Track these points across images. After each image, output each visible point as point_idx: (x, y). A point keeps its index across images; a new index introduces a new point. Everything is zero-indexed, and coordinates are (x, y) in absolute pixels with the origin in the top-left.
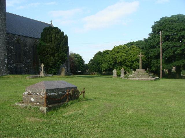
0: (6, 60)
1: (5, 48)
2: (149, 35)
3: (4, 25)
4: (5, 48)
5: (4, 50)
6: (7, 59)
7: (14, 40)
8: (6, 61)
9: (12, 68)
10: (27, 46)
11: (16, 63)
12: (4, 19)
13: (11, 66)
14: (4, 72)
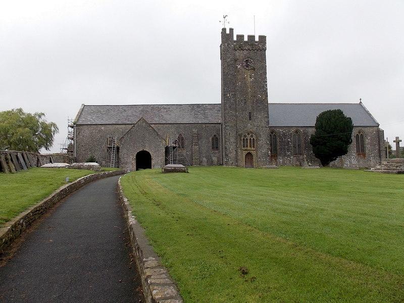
0: (270, 152)
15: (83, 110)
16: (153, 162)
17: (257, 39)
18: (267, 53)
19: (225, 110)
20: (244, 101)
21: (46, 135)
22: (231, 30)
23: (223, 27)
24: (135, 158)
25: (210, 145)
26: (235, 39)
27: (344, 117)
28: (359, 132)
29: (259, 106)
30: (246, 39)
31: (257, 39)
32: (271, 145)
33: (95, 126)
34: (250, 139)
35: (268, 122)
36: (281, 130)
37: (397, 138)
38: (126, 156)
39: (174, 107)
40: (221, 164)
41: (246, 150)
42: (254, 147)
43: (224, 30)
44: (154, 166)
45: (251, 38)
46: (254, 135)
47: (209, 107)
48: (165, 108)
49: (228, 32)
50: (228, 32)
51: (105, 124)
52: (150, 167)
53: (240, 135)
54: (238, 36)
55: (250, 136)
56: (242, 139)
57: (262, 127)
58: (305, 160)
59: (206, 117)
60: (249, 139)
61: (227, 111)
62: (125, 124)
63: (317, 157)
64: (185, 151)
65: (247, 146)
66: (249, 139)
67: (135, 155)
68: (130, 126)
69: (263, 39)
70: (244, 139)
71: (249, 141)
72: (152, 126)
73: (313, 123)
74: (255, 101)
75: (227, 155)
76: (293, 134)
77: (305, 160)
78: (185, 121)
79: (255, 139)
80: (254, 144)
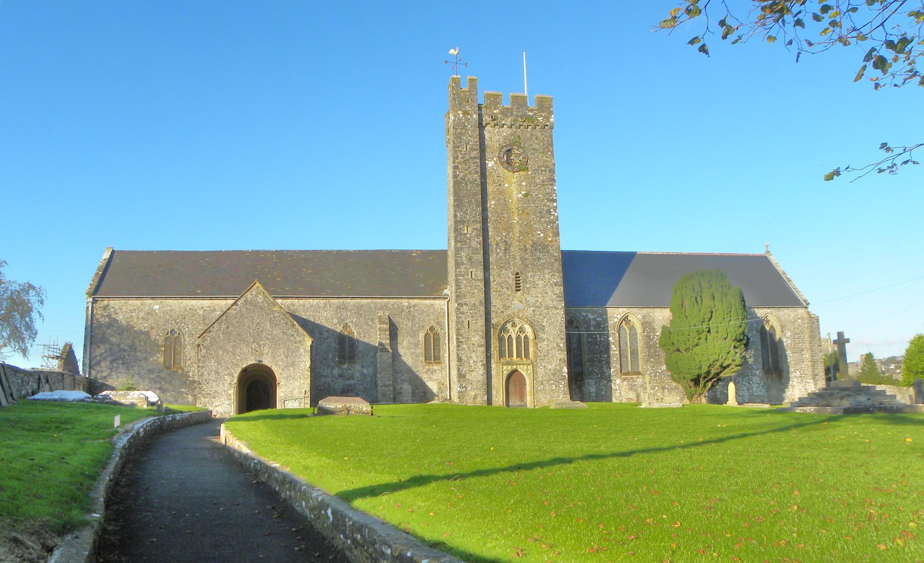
15: (109, 261)
24: (235, 381)
25: (421, 350)
29: (539, 259)
34: (518, 337)
37: (840, 335)
38: (213, 376)
40: (552, 171)
55: (517, 329)
57: (547, 308)
60: (514, 337)
61: (463, 268)
63: (674, 380)
64: (357, 367)
66: (514, 337)
74: (528, 246)
79: (531, 336)
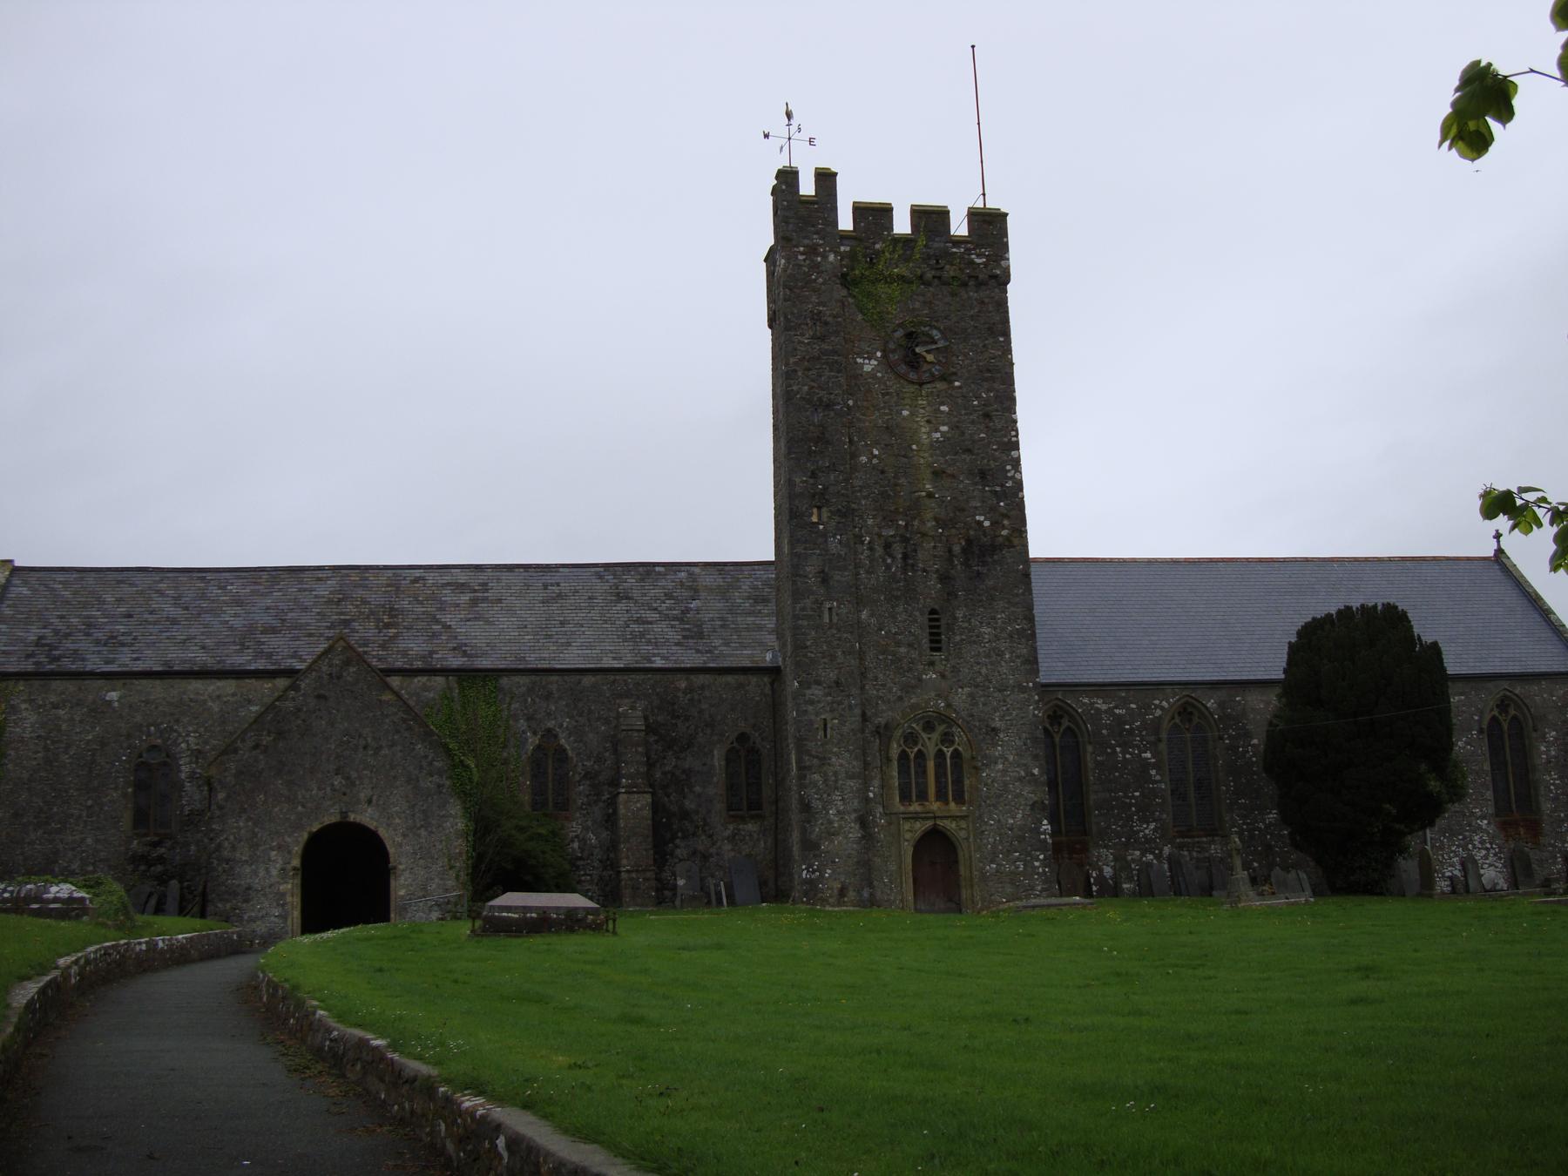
0: (1046, 826)
1: (1036, 771)
2: (1552, 526)
3: (1023, 663)
4: (1036, 771)
5: (1033, 780)
6: (1050, 823)
7: (1158, 713)
8: (1044, 833)
9: (1149, 864)
10: (1248, 735)
11: (1182, 835)
12: (1021, 633)
13: (1143, 855)
14: (1033, 889)
16: (400, 887)
17: (959, 226)
18: (1015, 293)
19: (797, 595)
20: (898, 550)
21: (1332, 615)
22: (826, 179)
23: (782, 162)
24: (296, 862)
26: (845, 222)
27: (1409, 638)
28: (1503, 705)
30: (902, 225)
31: (959, 226)
32: (1052, 784)
33: (71, 686)
34: (940, 754)
35: (1032, 662)
36: (1101, 704)
39: (265, 576)
41: (915, 817)
42: (959, 799)
43: (787, 178)
44: (403, 909)
45: (930, 219)
46: (960, 738)
47: (708, 580)
48: (460, 587)
49: (807, 187)
50: (807, 187)
51: (406, 670)
52: (385, 918)
53: (884, 732)
54: (860, 210)
55: (936, 736)
56: (895, 750)
58: (1238, 862)
59: (305, 661)
60: (931, 751)
62: (239, 674)
65: (923, 796)
66: (931, 751)
67: (297, 849)
68: (282, 683)
69: (989, 225)
70: (903, 756)
71: (931, 765)
72: (395, 681)
73: (1275, 667)
75: (810, 846)
76: (1165, 725)
77: (1238, 862)
78: (572, 658)
79: (966, 755)
80: (958, 782)
